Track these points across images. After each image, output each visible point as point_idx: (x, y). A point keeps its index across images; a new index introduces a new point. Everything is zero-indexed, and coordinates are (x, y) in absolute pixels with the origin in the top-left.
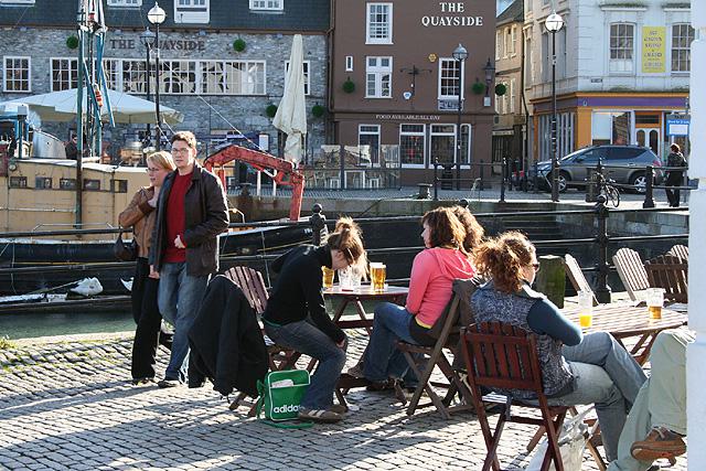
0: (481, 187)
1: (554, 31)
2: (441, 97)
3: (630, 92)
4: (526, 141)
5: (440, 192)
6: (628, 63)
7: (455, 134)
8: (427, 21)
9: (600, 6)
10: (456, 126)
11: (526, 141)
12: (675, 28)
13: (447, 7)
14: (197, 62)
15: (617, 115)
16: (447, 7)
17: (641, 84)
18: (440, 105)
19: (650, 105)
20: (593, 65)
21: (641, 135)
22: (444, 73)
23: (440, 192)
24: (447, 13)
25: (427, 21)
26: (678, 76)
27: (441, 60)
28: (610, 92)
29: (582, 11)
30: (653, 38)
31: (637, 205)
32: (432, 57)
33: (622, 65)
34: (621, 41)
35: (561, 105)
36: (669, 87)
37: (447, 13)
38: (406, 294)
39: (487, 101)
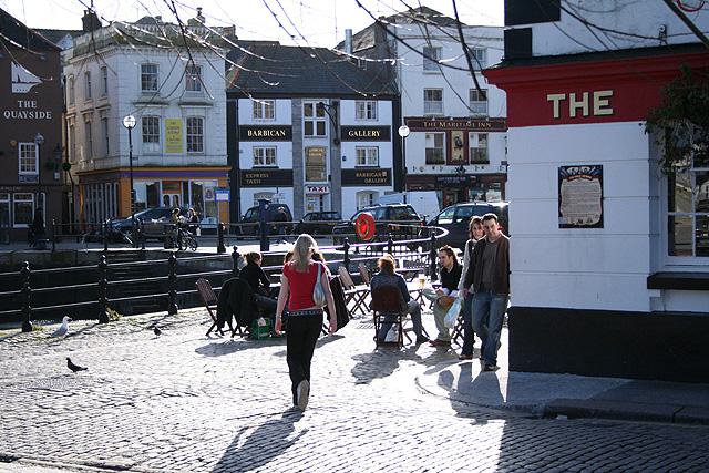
0: (88, 240)
1: (130, 128)
2: (21, 173)
3: (179, 167)
4: (72, 204)
5: (56, 245)
6: (157, 146)
7: (9, 201)
8: (8, 115)
9: (134, 104)
10: (33, 195)
11: (72, 204)
12: (189, 120)
13: (23, 104)
14: (171, 196)
15: (149, 184)
16: (23, 104)
17: (166, 161)
18: (21, 178)
19: (176, 176)
20: (129, 144)
21: (167, 198)
22: (34, 162)
23: (56, 245)
24: (24, 109)
25: (8, 115)
26: (191, 155)
27: (20, 144)
28: (144, 167)
29: (121, 107)
30: (173, 128)
31: (177, 250)
32: (13, 142)
33: (152, 147)
34: (150, 129)
35: (105, 178)
36: (186, 163)
37: (24, 109)
38: (279, 288)
39: (57, 175)
